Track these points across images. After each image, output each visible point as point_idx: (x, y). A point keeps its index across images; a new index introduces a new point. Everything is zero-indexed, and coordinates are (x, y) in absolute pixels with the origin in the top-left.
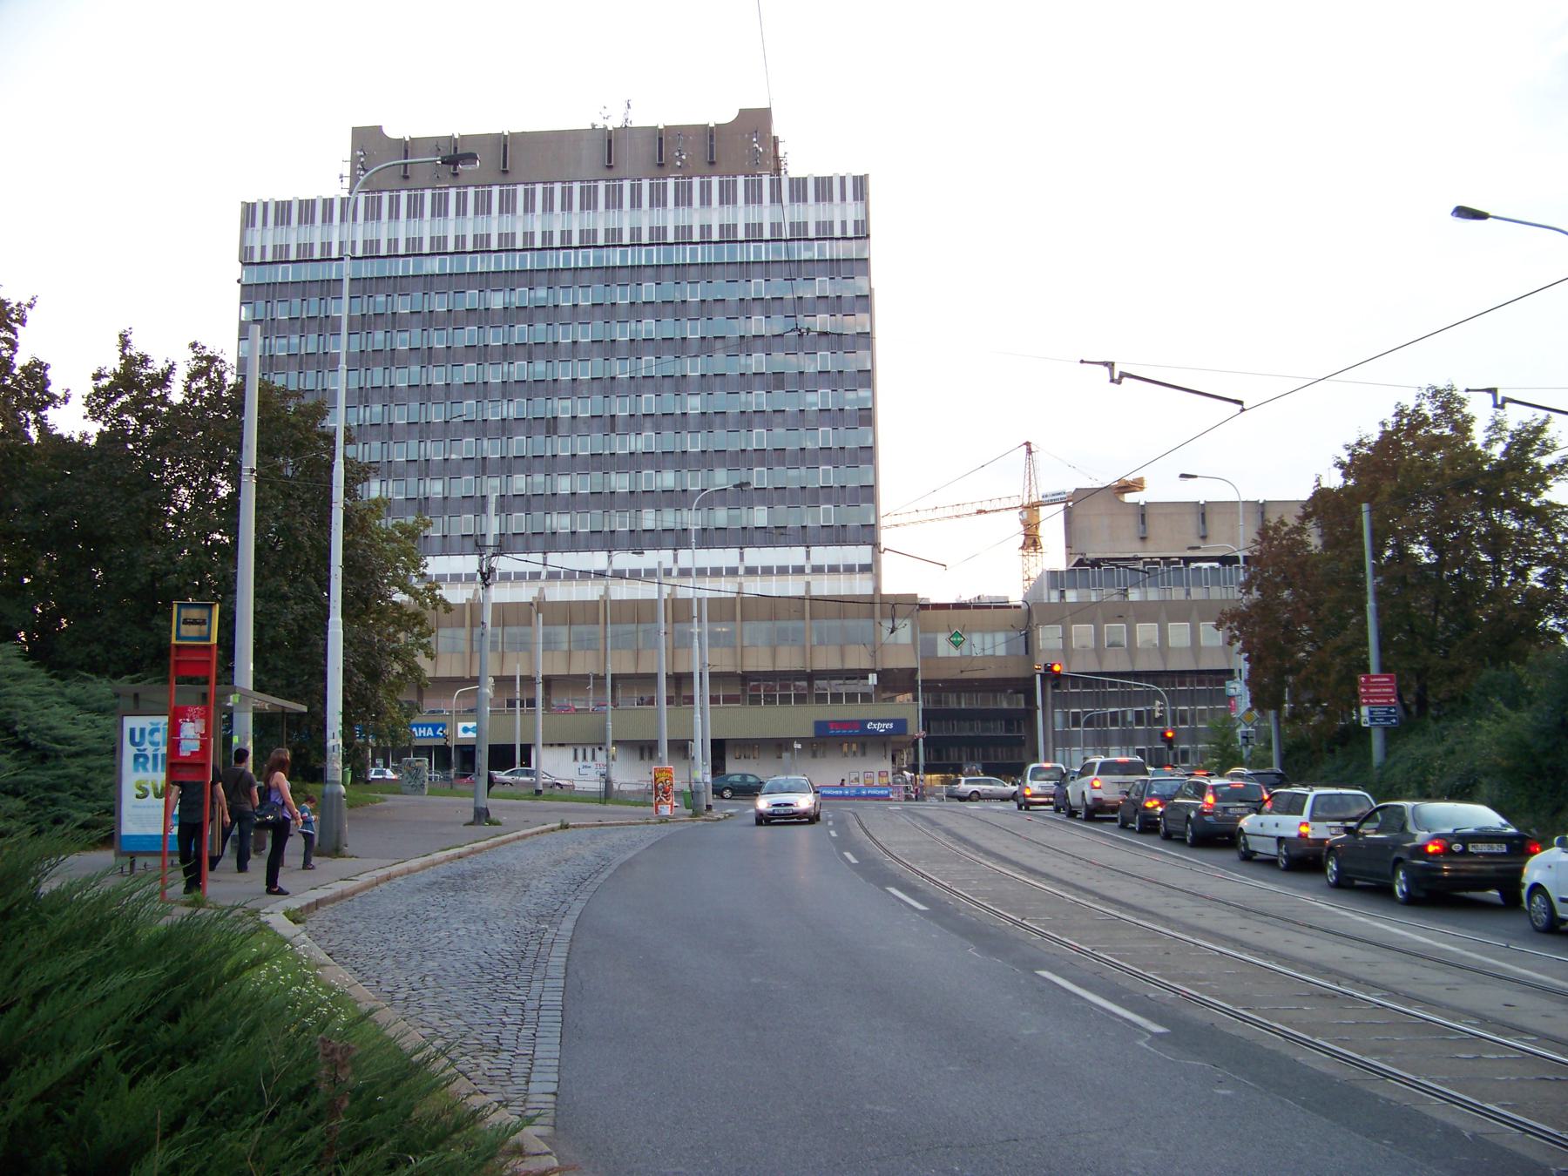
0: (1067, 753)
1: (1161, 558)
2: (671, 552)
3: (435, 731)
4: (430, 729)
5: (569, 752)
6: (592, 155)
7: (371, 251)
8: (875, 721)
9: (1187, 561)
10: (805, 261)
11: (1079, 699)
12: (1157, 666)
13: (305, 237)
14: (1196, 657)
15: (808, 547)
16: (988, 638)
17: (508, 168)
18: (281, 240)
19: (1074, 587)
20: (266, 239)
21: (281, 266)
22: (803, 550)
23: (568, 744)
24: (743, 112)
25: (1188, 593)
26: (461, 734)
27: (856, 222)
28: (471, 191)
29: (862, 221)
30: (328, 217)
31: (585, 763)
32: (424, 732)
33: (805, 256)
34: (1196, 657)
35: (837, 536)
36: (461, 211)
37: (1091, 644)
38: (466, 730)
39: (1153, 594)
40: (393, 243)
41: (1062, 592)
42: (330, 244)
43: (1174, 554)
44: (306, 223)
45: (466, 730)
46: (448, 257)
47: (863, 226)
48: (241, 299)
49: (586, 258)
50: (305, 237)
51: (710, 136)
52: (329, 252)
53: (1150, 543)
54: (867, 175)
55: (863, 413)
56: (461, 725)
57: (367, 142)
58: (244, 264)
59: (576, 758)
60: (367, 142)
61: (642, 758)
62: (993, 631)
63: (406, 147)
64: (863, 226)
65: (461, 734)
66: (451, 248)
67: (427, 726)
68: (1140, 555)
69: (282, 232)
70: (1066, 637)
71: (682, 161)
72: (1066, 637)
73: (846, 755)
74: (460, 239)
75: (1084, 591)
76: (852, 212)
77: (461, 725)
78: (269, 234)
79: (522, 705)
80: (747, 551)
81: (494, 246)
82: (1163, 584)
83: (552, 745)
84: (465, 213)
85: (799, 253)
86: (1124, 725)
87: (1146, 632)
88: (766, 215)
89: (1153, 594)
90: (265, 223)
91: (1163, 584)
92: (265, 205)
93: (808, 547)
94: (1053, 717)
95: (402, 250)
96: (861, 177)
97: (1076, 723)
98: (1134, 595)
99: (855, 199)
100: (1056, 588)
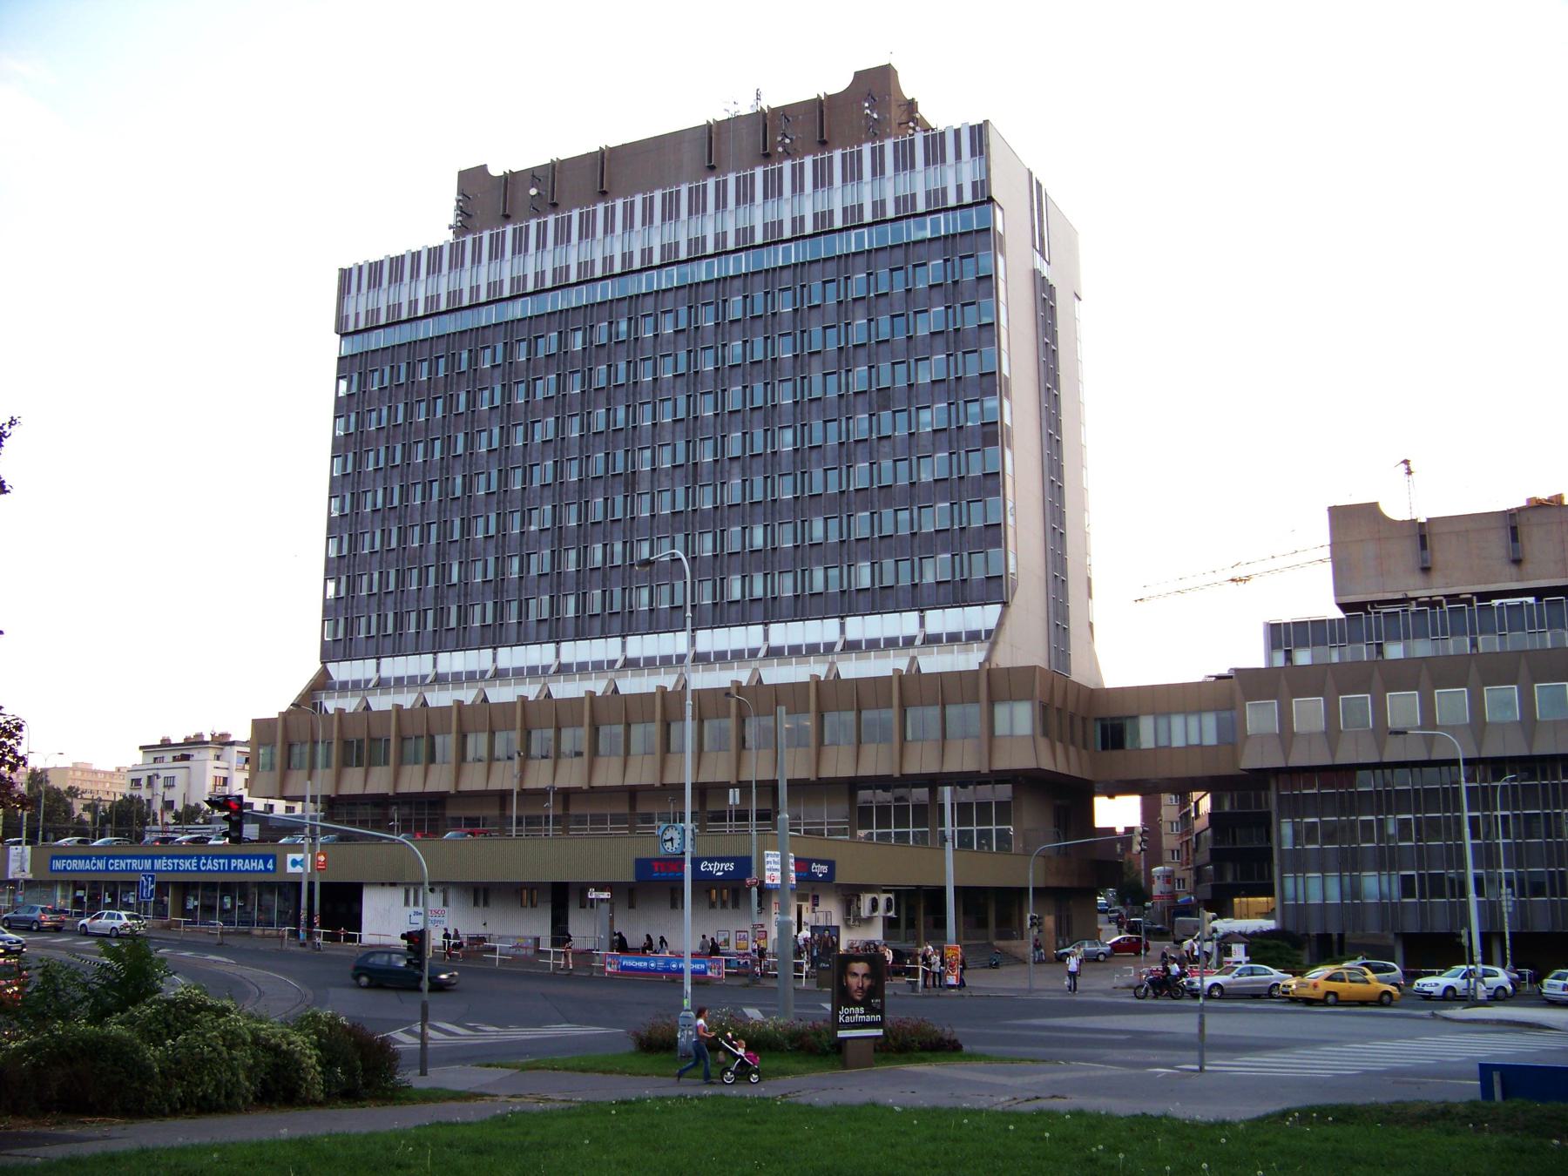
0: (1300, 881)
1: (1473, 594)
2: (760, 628)
3: (266, 863)
4: (261, 861)
5: (399, 894)
6: (691, 156)
7: (905, 209)
8: (711, 860)
9: (1485, 596)
10: (915, 243)
11: (1317, 805)
12: (1518, 749)
13: (936, 180)
14: (1530, 736)
15: (922, 611)
16: (1193, 721)
17: (825, 138)
18: (905, 190)
19: (1396, 638)
20: (360, 305)
21: (853, 233)
22: (915, 615)
23: (400, 884)
24: (858, 75)
25: (1474, 644)
26: (290, 869)
27: (974, 184)
28: (808, 161)
29: (982, 181)
30: (415, 273)
31: (416, 909)
32: (255, 864)
33: (917, 235)
34: (1530, 736)
35: (957, 594)
36: (878, 169)
37: (1321, 725)
38: (295, 863)
39: (1422, 648)
40: (798, 222)
41: (1380, 646)
42: (802, 218)
43: (1465, 589)
44: (905, 168)
45: (295, 863)
46: (865, 230)
47: (982, 188)
48: (338, 373)
49: (670, 277)
50: (936, 180)
51: (820, 109)
52: (884, 212)
53: (1436, 577)
54: (986, 122)
55: (987, 429)
56: (290, 857)
57: (473, 183)
58: (343, 335)
59: (407, 903)
60: (473, 183)
61: (476, 904)
62: (1199, 711)
63: (510, 179)
64: (982, 188)
65: (290, 869)
66: (868, 218)
67: (258, 857)
68: (1411, 595)
69: (561, 252)
70: (1285, 716)
71: (784, 146)
72: (1285, 716)
73: (712, 905)
74: (879, 206)
75: (1320, 649)
76: (968, 172)
77: (290, 857)
78: (362, 300)
79: (547, 817)
80: (929, 614)
81: (921, 208)
82: (1531, 626)
83: (383, 884)
84: (882, 172)
85: (909, 235)
86: (1381, 840)
87: (1403, 707)
88: (920, 183)
89: (1422, 648)
90: (958, 156)
91: (1531, 626)
92: (957, 132)
93: (922, 611)
94: (1279, 830)
95: (731, 246)
96: (980, 126)
97: (1311, 838)
98: (1394, 651)
99: (973, 154)
100: (1280, 647)
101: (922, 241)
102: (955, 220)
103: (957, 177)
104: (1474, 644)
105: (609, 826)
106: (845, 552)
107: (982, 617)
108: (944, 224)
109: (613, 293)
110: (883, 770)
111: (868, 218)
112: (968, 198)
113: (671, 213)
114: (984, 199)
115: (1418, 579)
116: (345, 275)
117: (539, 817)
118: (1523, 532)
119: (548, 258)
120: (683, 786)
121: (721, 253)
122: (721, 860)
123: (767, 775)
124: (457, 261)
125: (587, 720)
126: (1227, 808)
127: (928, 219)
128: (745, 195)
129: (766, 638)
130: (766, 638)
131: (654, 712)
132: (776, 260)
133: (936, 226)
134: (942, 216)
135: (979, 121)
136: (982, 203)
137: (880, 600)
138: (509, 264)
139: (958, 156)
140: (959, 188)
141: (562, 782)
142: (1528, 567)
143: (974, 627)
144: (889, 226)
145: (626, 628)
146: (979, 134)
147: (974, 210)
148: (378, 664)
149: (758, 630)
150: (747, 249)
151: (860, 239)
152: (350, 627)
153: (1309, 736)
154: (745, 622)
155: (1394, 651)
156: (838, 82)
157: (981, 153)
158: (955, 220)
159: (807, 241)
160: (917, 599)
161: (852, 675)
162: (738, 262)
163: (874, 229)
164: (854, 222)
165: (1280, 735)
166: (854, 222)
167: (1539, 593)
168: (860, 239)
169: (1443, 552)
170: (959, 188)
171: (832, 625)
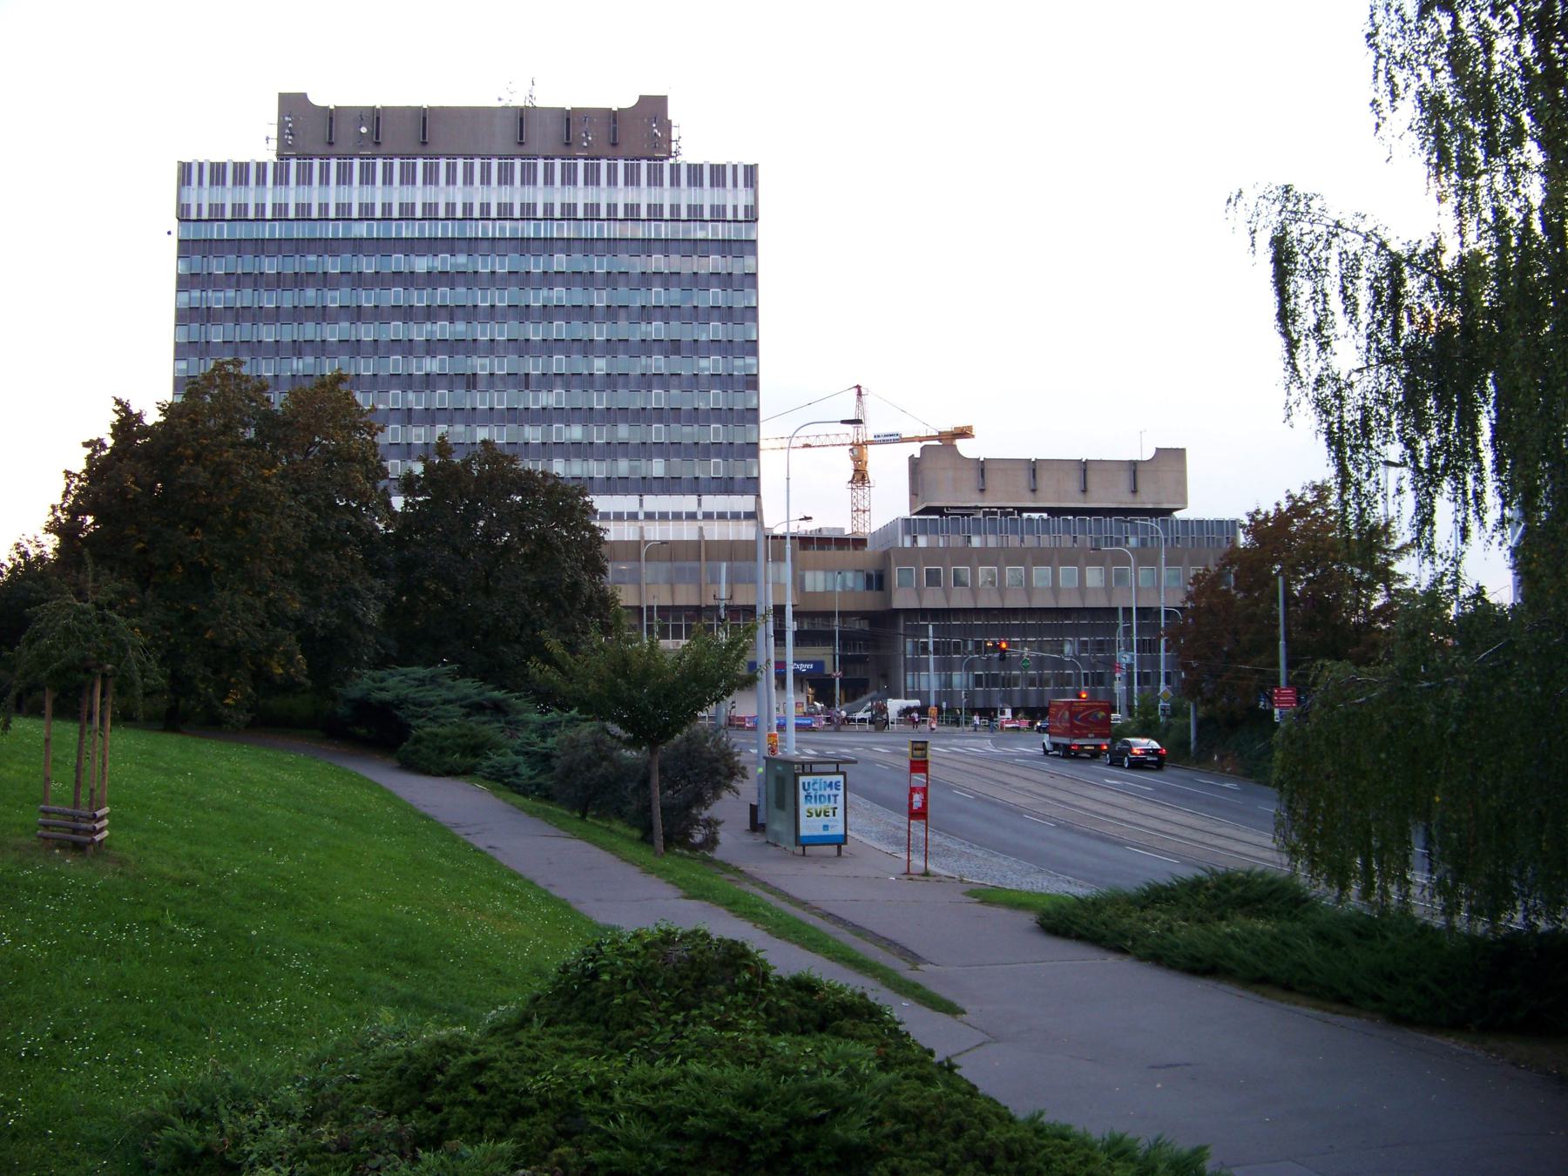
1: (1014, 508)
9: (1021, 510)
21: (216, 224)
22: (694, 498)
25: (1022, 540)
30: (261, 180)
33: (700, 235)
35: (726, 486)
40: (260, 208)
41: (915, 537)
58: (180, 220)
63: (332, 116)
76: (743, 197)
80: (704, 498)
88: (666, 196)
89: (992, 541)
97: (957, 645)
102: (729, 229)
104: (1022, 540)
107: (743, 503)
108: (722, 231)
109: (280, 233)
112: (205, 216)
113: (569, 178)
115: (977, 496)
118: (1089, 473)
122: (804, 662)
123: (633, 602)
124: (281, 178)
126: (806, 628)
128: (344, 178)
129: (641, 505)
130: (641, 505)
132: (413, 232)
135: (751, 163)
137: (669, 485)
142: (987, 493)
143: (736, 509)
146: (751, 172)
153: (1095, 590)
154: (626, 491)
155: (976, 542)
156: (628, 101)
160: (697, 487)
162: (560, 228)
164: (367, 214)
165: (1105, 588)
166: (367, 214)
167: (1052, 512)
169: (993, 480)
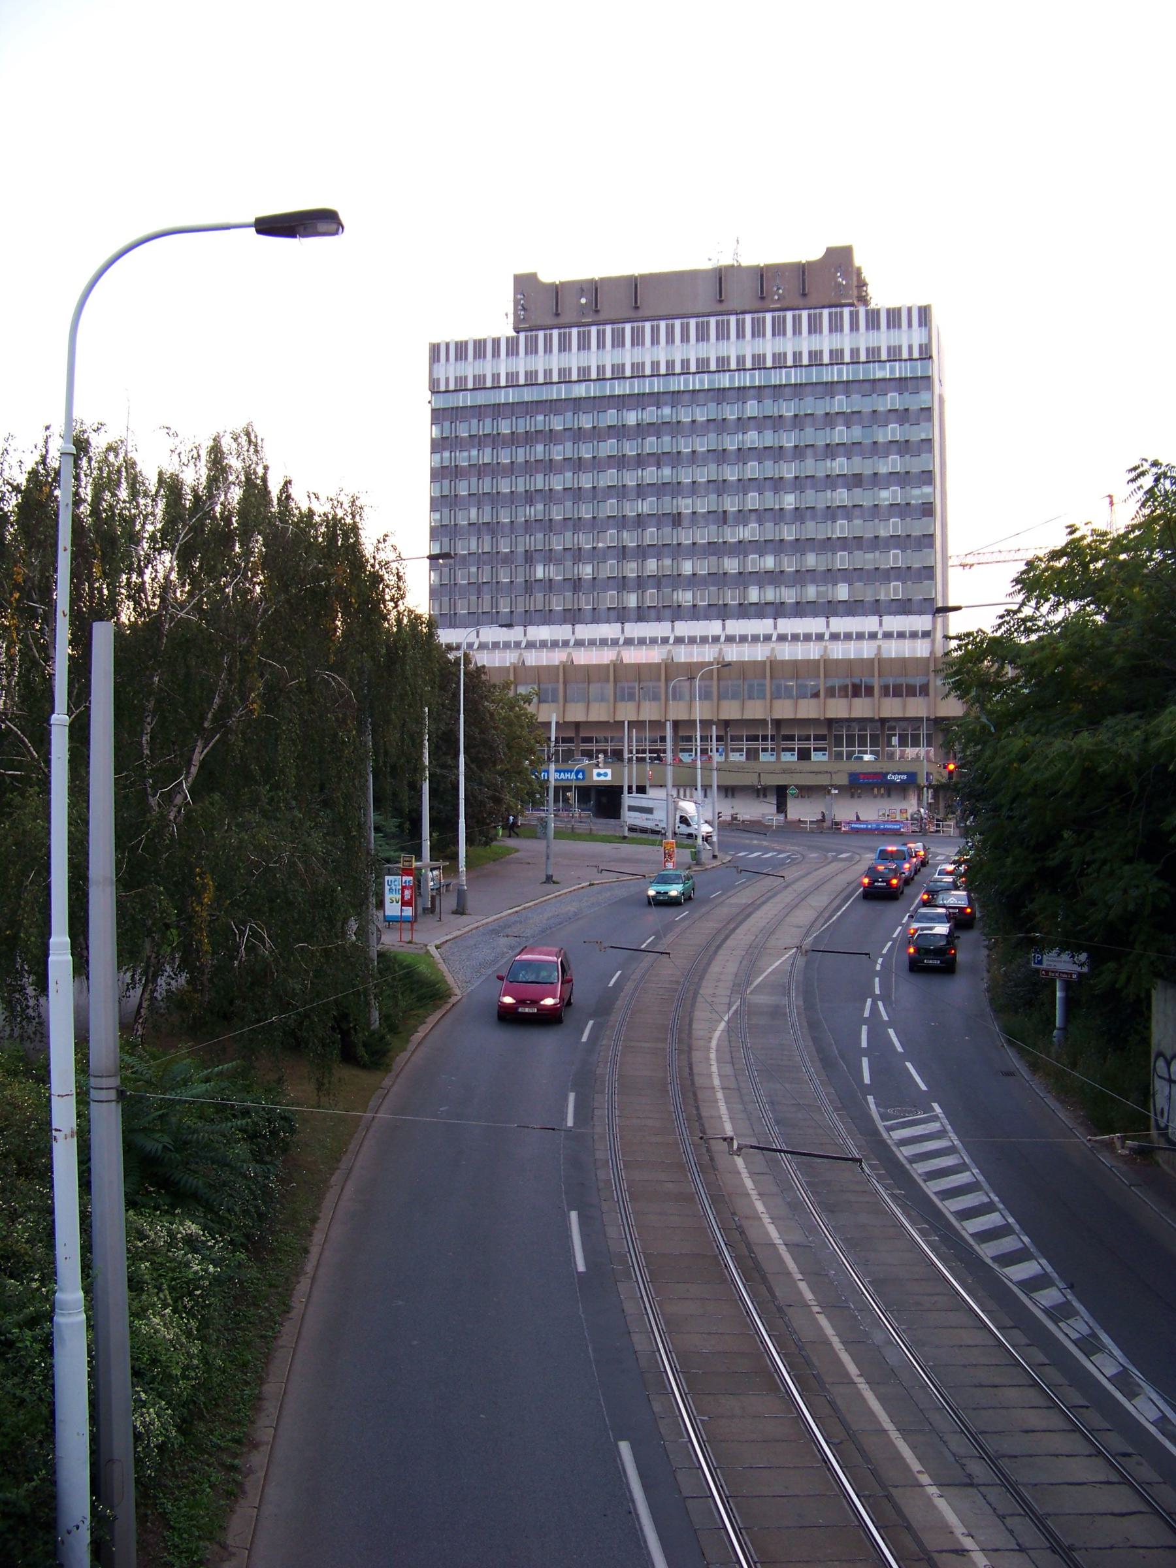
20: (449, 371)
21: (836, 367)
22: (876, 618)
27: (921, 346)
30: (496, 353)
35: (904, 607)
40: (495, 377)
49: (702, 382)
55: (926, 506)
58: (433, 393)
73: (875, 797)
76: (917, 337)
78: (451, 369)
85: (874, 373)
88: (864, 340)
90: (910, 325)
92: (447, 345)
99: (920, 325)
101: (884, 380)
102: (906, 368)
103: (909, 338)
105: (659, 743)
106: (831, 576)
109: (659, 387)
110: (603, 718)
111: (470, 386)
114: (926, 355)
116: (435, 350)
117: (691, 737)
119: (451, 369)
120: (550, 723)
121: (741, 369)
125: (612, 678)
127: (888, 364)
128: (618, 342)
130: (724, 629)
131: (608, 676)
133: (892, 370)
134: (897, 364)
136: (925, 359)
138: (453, 367)
139: (910, 325)
140: (910, 348)
141: (724, 716)
144: (861, 366)
145: (528, 621)
146: (925, 314)
147: (919, 363)
148: (573, 629)
149: (822, 621)
150: (513, 386)
151: (840, 372)
152: (453, 604)
157: (926, 325)
158: (906, 368)
159: (804, 369)
161: (582, 662)
163: (851, 366)
168: (840, 372)
170: (447, 380)
171: (821, 621)
